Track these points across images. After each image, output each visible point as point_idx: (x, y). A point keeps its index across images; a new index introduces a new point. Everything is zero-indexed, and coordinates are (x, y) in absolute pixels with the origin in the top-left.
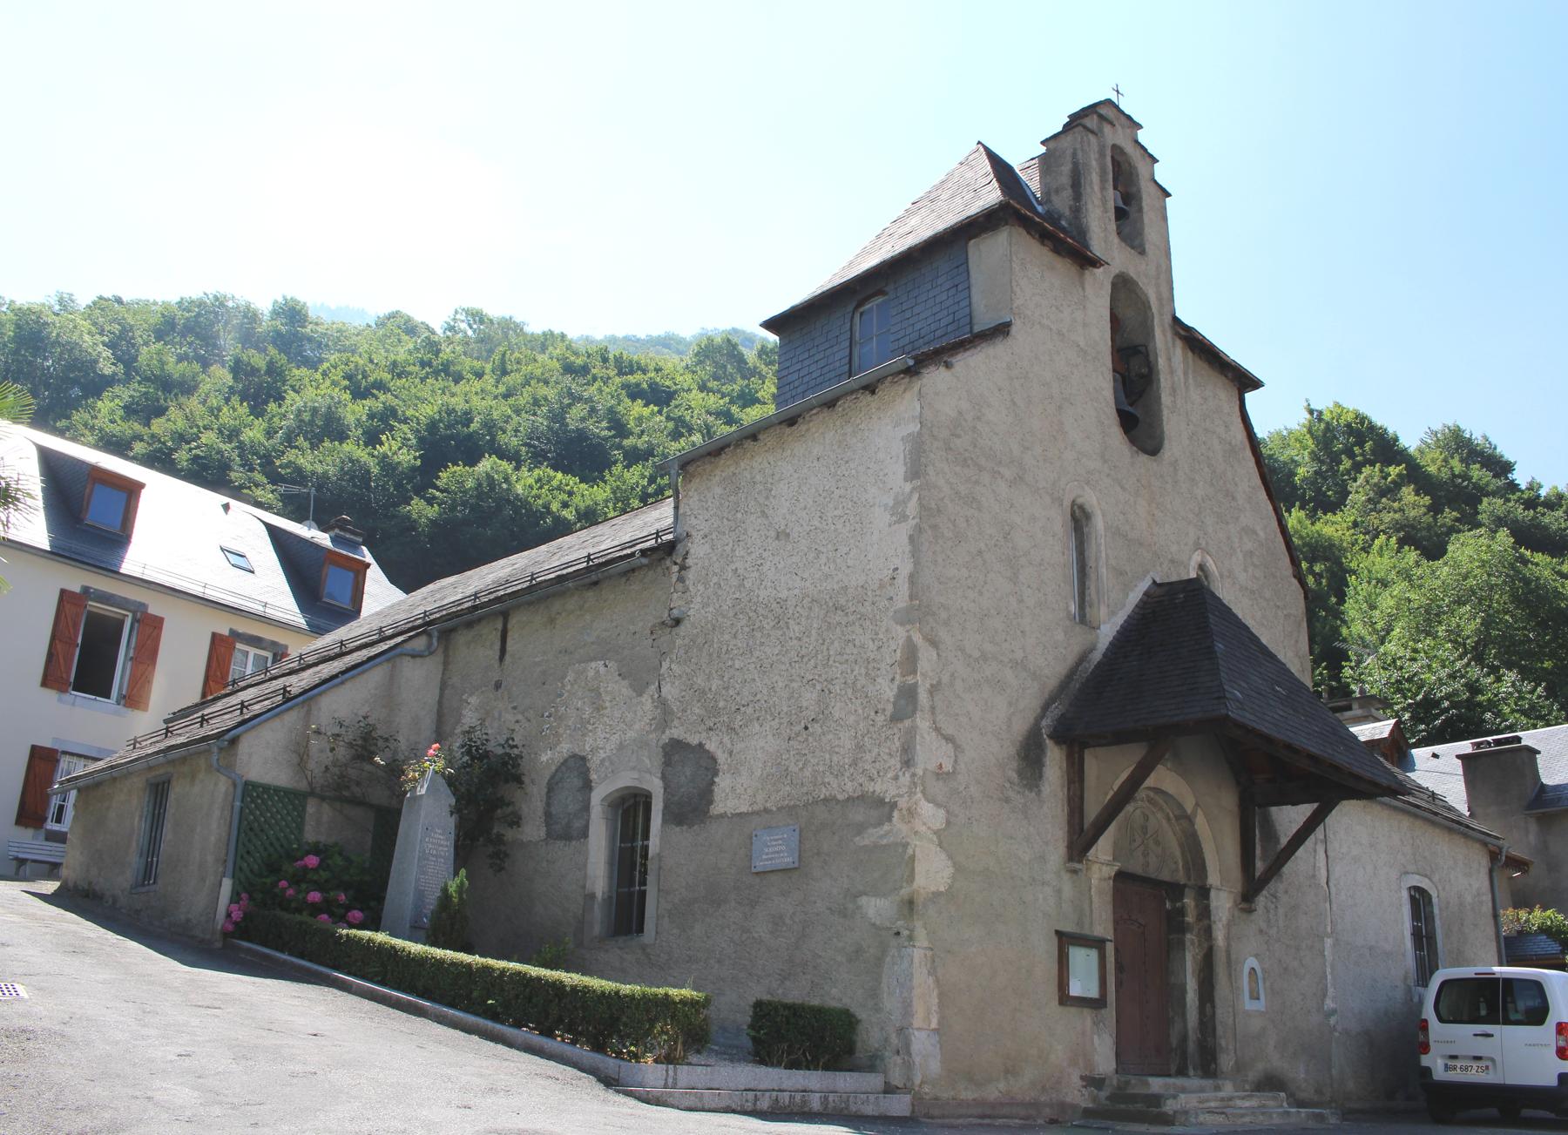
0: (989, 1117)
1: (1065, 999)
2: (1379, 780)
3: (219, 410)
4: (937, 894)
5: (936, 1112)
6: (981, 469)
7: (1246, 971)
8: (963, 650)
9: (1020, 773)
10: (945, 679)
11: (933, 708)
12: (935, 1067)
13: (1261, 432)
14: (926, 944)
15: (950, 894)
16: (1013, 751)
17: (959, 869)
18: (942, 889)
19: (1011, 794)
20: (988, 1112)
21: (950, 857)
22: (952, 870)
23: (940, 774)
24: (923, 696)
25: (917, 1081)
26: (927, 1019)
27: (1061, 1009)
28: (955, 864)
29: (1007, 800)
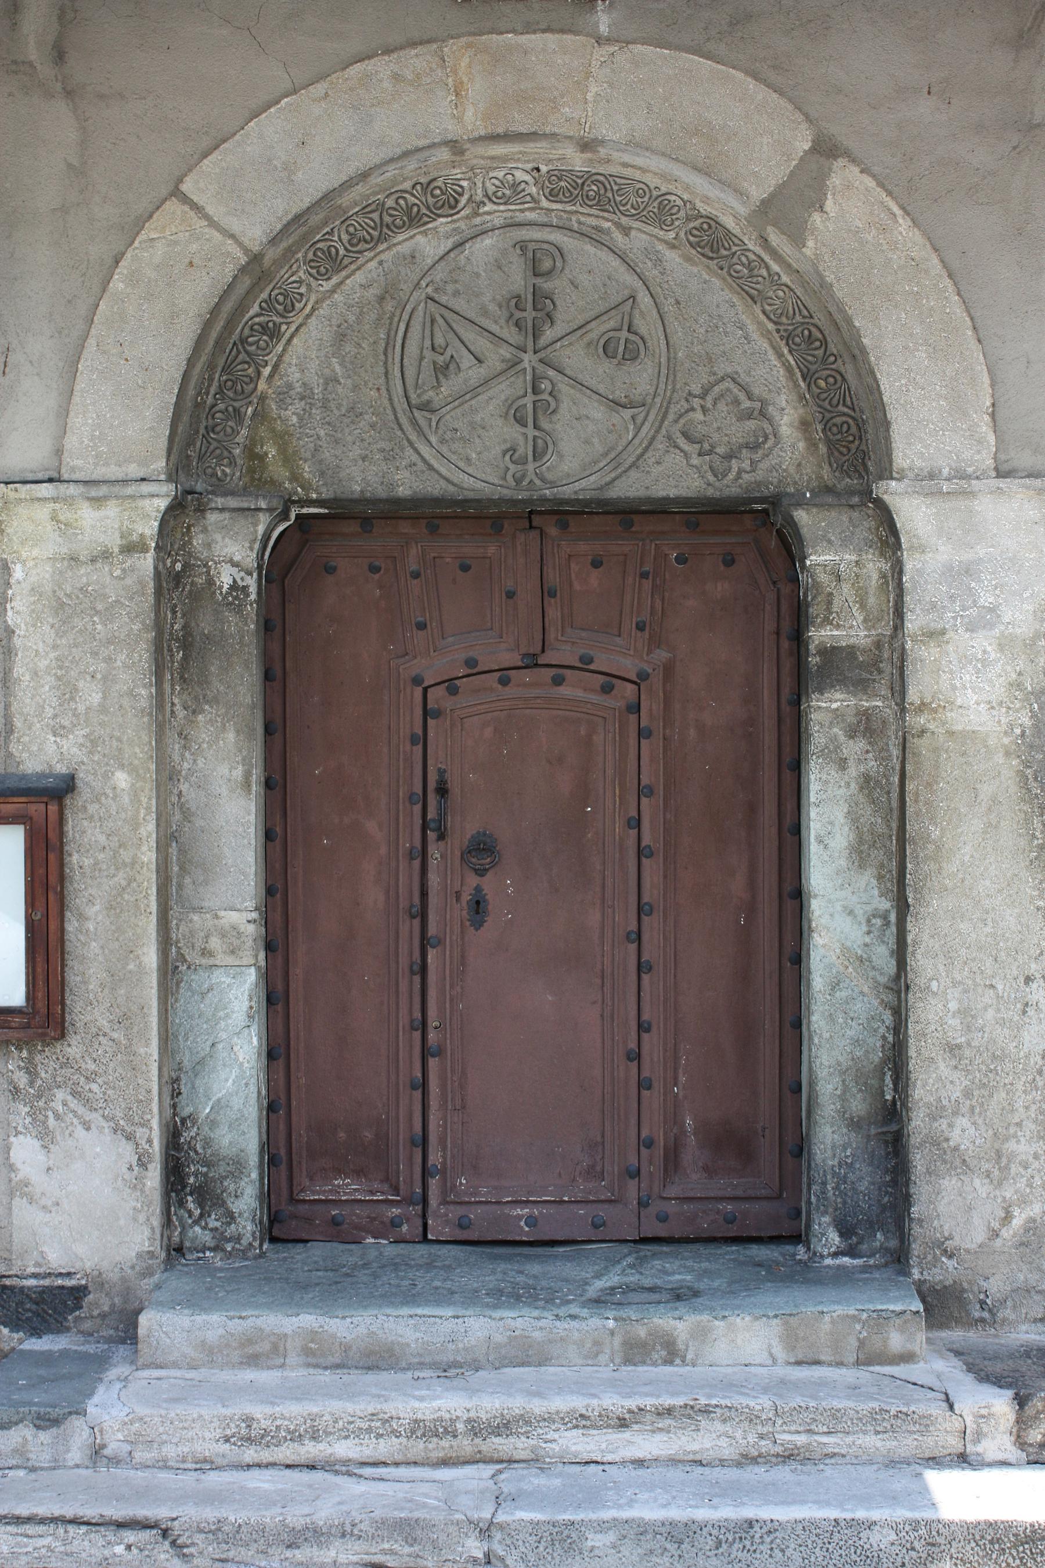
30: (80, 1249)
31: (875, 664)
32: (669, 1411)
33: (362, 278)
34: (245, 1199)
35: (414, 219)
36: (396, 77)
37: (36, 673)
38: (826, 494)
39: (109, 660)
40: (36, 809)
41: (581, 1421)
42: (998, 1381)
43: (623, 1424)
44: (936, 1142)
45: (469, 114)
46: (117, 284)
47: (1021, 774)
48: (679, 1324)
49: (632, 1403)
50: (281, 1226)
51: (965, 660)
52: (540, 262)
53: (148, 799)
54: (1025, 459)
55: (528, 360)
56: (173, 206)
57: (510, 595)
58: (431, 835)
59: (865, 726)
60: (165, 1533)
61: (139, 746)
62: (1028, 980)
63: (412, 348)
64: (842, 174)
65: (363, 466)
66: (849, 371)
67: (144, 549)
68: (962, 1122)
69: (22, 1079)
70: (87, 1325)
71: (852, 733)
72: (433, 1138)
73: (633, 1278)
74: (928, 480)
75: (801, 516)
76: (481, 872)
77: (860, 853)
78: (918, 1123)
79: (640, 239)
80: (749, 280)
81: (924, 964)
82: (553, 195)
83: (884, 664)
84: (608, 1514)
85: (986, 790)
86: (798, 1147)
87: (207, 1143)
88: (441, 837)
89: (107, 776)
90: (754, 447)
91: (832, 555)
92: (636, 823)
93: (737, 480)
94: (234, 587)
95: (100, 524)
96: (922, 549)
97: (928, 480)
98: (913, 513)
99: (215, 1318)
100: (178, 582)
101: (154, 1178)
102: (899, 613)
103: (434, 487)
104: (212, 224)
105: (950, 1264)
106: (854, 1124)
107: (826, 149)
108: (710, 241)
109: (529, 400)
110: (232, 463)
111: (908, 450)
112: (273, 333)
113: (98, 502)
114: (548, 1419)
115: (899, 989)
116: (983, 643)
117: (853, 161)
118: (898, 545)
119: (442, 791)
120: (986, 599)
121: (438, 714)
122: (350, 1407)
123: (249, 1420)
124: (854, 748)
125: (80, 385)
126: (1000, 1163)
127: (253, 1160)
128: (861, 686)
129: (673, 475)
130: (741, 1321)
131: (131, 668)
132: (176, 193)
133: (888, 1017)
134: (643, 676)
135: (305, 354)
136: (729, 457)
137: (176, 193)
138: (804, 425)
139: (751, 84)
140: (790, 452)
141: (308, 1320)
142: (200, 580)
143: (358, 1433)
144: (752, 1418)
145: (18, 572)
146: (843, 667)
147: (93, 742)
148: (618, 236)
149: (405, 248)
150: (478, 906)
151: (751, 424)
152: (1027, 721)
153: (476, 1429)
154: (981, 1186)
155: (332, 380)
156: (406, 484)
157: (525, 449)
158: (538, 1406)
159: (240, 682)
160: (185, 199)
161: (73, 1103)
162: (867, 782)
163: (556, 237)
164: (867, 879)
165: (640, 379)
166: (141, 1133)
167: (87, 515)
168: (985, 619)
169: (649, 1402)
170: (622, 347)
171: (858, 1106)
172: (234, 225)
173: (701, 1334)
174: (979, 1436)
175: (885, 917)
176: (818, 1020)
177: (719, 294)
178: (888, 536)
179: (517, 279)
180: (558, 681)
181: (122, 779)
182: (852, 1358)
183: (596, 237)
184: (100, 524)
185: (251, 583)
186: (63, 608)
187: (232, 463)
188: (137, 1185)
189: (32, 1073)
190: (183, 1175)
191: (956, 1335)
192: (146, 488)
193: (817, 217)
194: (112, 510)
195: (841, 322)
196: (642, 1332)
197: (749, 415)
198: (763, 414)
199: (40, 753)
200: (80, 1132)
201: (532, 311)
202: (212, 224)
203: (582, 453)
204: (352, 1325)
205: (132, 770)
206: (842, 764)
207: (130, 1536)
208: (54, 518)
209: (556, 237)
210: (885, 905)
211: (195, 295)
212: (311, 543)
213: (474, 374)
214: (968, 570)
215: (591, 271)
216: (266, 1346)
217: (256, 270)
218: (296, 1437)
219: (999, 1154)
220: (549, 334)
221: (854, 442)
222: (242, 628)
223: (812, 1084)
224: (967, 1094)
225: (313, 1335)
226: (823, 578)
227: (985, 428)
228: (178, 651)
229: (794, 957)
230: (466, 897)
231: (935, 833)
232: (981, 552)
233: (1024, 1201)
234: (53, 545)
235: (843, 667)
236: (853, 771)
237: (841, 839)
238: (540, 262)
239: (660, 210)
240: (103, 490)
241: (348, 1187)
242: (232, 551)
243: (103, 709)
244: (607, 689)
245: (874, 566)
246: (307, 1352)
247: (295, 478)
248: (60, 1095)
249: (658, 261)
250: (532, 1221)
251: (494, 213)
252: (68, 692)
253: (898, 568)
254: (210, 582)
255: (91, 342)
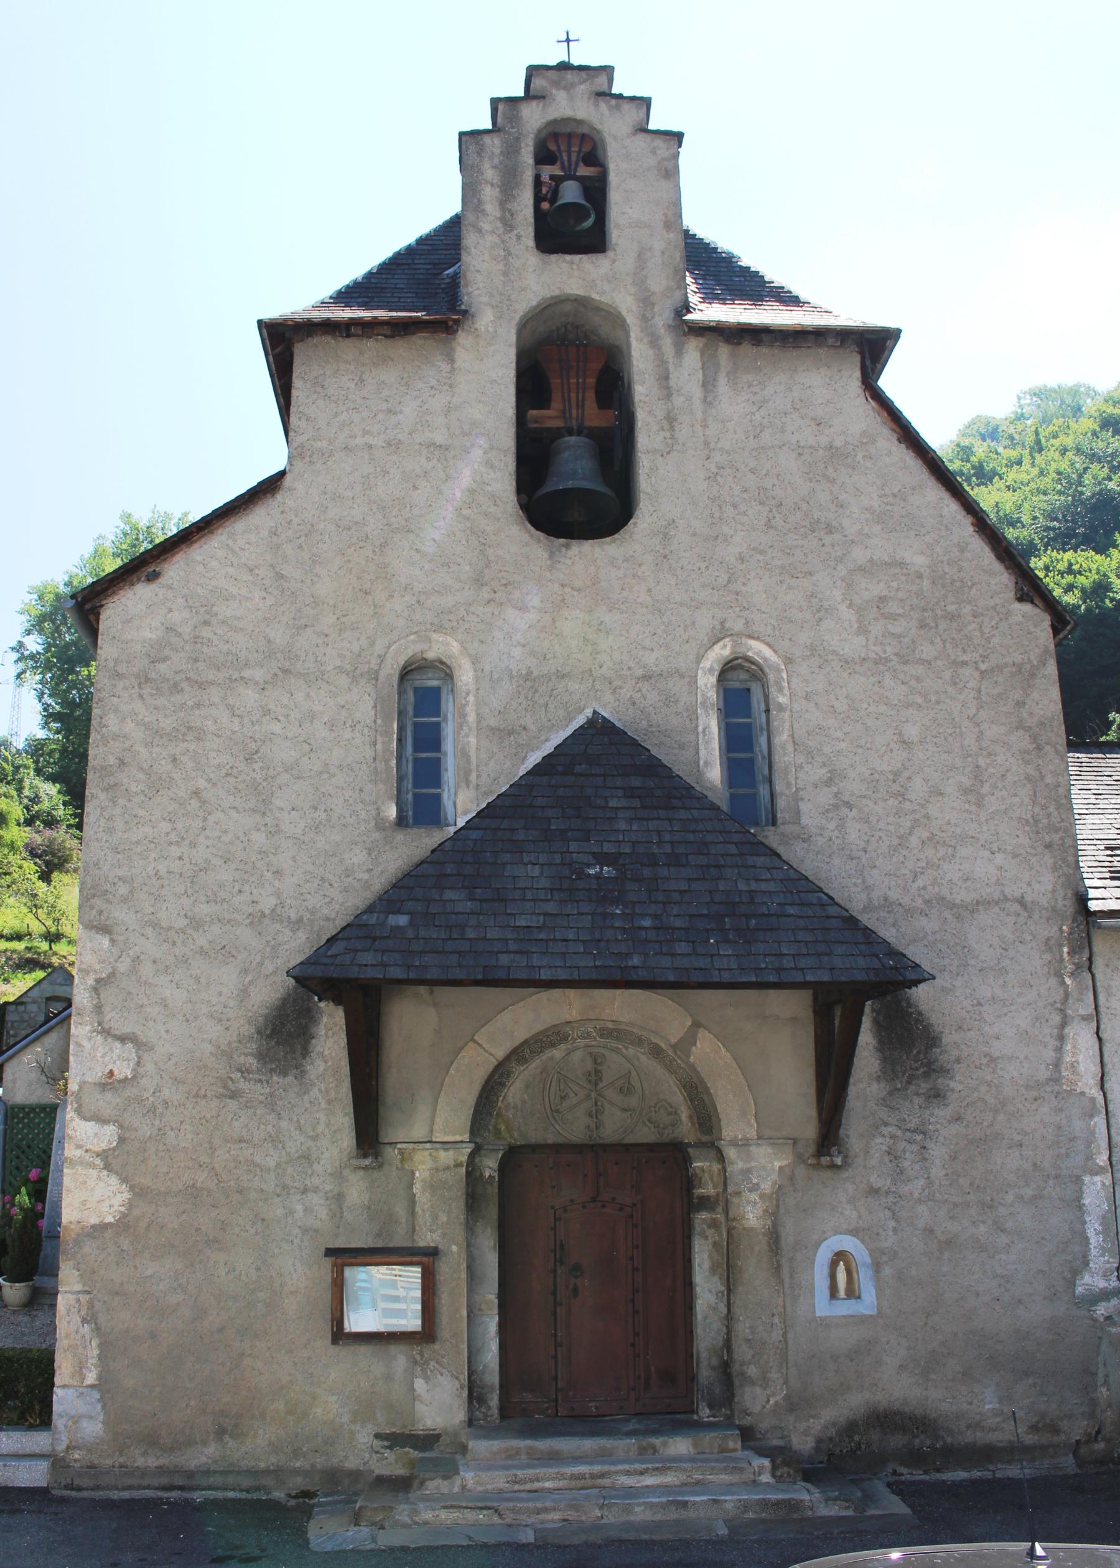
0: (181, 1488)
1: (339, 1335)
2: (884, 955)
3: (500, 679)
4: (103, 1227)
5: (85, 1482)
6: (202, 686)
7: (823, 1256)
8: (155, 925)
9: (261, 1056)
10: (124, 966)
11: (98, 1008)
12: (93, 1429)
13: (939, 436)
14: (78, 1287)
15: (123, 1225)
16: (248, 1030)
17: (139, 1193)
18: (110, 1219)
19: (242, 1085)
20: (179, 1481)
21: (124, 1180)
22: (127, 1195)
23: (109, 1083)
24: (81, 996)
25: (63, 1446)
26: (80, 1370)
27: (337, 1348)
28: (132, 1188)
29: (234, 1095)
30: (438, 1420)
31: (717, 1201)
32: (657, 1469)
33: (534, 1066)
34: (494, 1401)
35: (553, 1045)
36: (548, 1000)
37: (423, 1210)
38: (700, 1145)
39: (450, 1205)
40: (425, 1259)
41: (628, 1473)
42: (766, 1456)
43: (642, 1473)
44: (743, 1374)
45: (574, 1012)
46: (452, 1071)
47: (769, 1243)
48: (657, 1441)
49: (644, 1466)
50: (505, 1412)
51: (748, 1202)
52: (597, 1059)
53: (464, 1256)
54: (767, 1133)
55: (593, 1095)
56: (471, 1044)
57: (586, 1175)
58: (558, 1264)
59: (714, 1224)
60: (496, 1511)
61: (459, 1233)
62: (773, 1315)
63: (552, 1090)
64: (702, 1034)
65: (534, 1132)
66: (706, 1098)
67: (462, 1166)
68: (752, 1367)
69: (418, 1357)
70: (442, 1448)
71: (709, 1227)
72: (559, 1377)
73: (637, 1426)
74: (734, 1143)
75: (690, 1150)
76: (576, 1277)
77: (713, 1269)
78: (736, 1368)
79: (631, 1051)
80: (670, 1067)
81: (737, 1310)
82: (601, 1036)
83: (722, 1202)
84: (641, 1500)
85: (757, 1248)
86: (692, 1378)
87: (481, 1380)
88: (562, 1264)
89: (449, 1248)
90: (673, 1125)
91: (700, 1164)
92: (632, 1259)
93: (667, 1136)
94: (490, 1176)
95: (446, 1157)
96: (733, 1163)
97: (734, 1143)
98: (731, 1153)
99: (496, 1442)
100: (472, 1175)
101: (465, 1394)
102: (725, 1184)
103: (561, 1140)
104: (485, 1050)
105: (749, 1418)
106: (713, 1368)
107: (697, 1025)
108: (656, 1052)
109: (594, 1109)
110: (489, 1131)
111: (727, 1133)
112: (503, 1085)
113: (446, 1150)
114: (616, 1472)
115: (729, 1318)
116: (754, 1196)
117: (706, 1029)
118: (724, 1161)
119: (562, 1246)
120: (755, 1181)
121: (560, 1219)
122: (550, 1470)
123: (516, 1475)
124: (710, 1232)
125: (439, 1107)
126: (765, 1382)
127: (498, 1386)
128: (712, 1209)
129: (645, 1135)
130: (678, 1439)
131: (458, 1207)
132: (473, 1040)
133: (725, 1329)
134: (634, 1205)
135: (514, 1092)
136: (665, 1128)
137: (473, 1040)
138: (691, 1117)
139: (670, 1002)
140: (686, 1130)
141: (528, 1442)
142: (478, 1174)
143: (553, 1479)
144: (685, 1470)
145: (417, 1174)
146: (705, 1203)
147: (444, 1235)
148: (624, 1050)
149: (549, 1055)
150: (575, 1290)
151: (672, 1117)
152: (769, 1223)
153: (593, 1476)
154: (758, 1390)
155: (524, 1102)
156: (551, 1139)
157: (593, 1126)
158: (613, 1468)
159: (493, 1212)
160: (475, 1042)
161: (437, 1366)
162: (715, 1244)
163: (602, 1051)
164: (716, 1279)
165: (634, 1101)
166: (461, 1377)
167: (442, 1154)
168: (755, 1188)
169: (650, 1466)
170: (626, 1090)
171: (715, 1362)
172: (493, 1051)
173: (665, 1444)
174: (760, 1474)
175: (723, 1293)
176: (699, 1331)
177: (660, 1071)
178: (721, 1158)
179: (589, 1065)
180: (604, 1206)
181: (454, 1248)
182: (716, 1451)
183: (616, 1051)
184: (446, 1157)
185: (496, 1174)
186: (432, 1187)
187: (489, 1131)
188: (460, 1396)
189: (421, 1354)
190: (475, 1394)
191: (752, 1444)
192: (464, 1145)
193: (694, 1048)
194: (451, 1152)
195: (702, 1081)
196: (644, 1444)
197: (670, 1114)
198: (676, 1113)
199: (426, 1239)
200: (439, 1376)
201: (595, 1076)
202: (485, 1050)
203: (614, 1126)
204: (543, 1445)
205: (457, 1244)
206: (706, 1238)
207: (485, 1512)
208: (430, 1154)
209: (602, 1051)
210: (723, 1288)
211: (480, 1075)
212: (512, 1158)
213: (575, 1100)
214: (749, 1171)
215: (614, 1065)
216: (514, 1452)
217: (500, 1065)
218: (532, 1481)
219: (764, 1378)
220: (600, 1085)
221: (706, 1119)
222: (493, 1191)
223: (698, 1354)
224: (753, 1357)
225: (530, 1448)
226: (698, 1171)
227: (753, 1121)
228: (473, 1201)
229: (690, 1307)
230: (571, 1287)
231: (740, 1263)
232: (753, 1164)
233: (774, 1395)
234: (430, 1164)
235: (705, 1203)
236: (710, 1240)
237: (707, 1265)
238: (597, 1059)
239: (639, 1041)
240: (449, 1146)
241: (529, 1397)
242: (490, 1166)
243: (447, 1223)
244: (621, 1210)
245: (716, 1167)
246: (528, 1453)
247: (511, 1137)
248: (432, 1363)
249: (638, 1059)
250: (596, 1408)
251: (580, 1042)
252: (435, 1217)
253: (724, 1170)
254: (481, 1175)
255: (443, 1093)
